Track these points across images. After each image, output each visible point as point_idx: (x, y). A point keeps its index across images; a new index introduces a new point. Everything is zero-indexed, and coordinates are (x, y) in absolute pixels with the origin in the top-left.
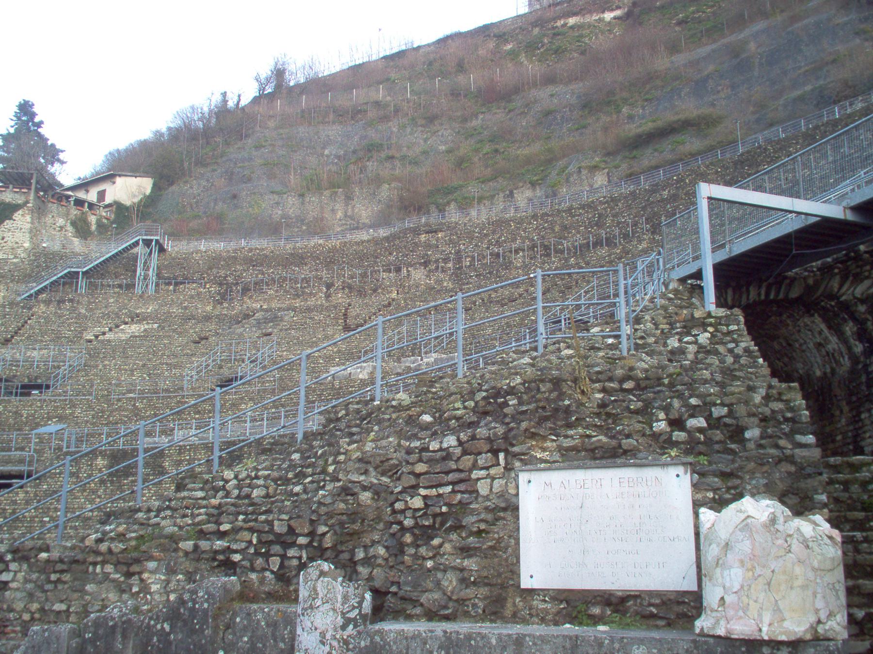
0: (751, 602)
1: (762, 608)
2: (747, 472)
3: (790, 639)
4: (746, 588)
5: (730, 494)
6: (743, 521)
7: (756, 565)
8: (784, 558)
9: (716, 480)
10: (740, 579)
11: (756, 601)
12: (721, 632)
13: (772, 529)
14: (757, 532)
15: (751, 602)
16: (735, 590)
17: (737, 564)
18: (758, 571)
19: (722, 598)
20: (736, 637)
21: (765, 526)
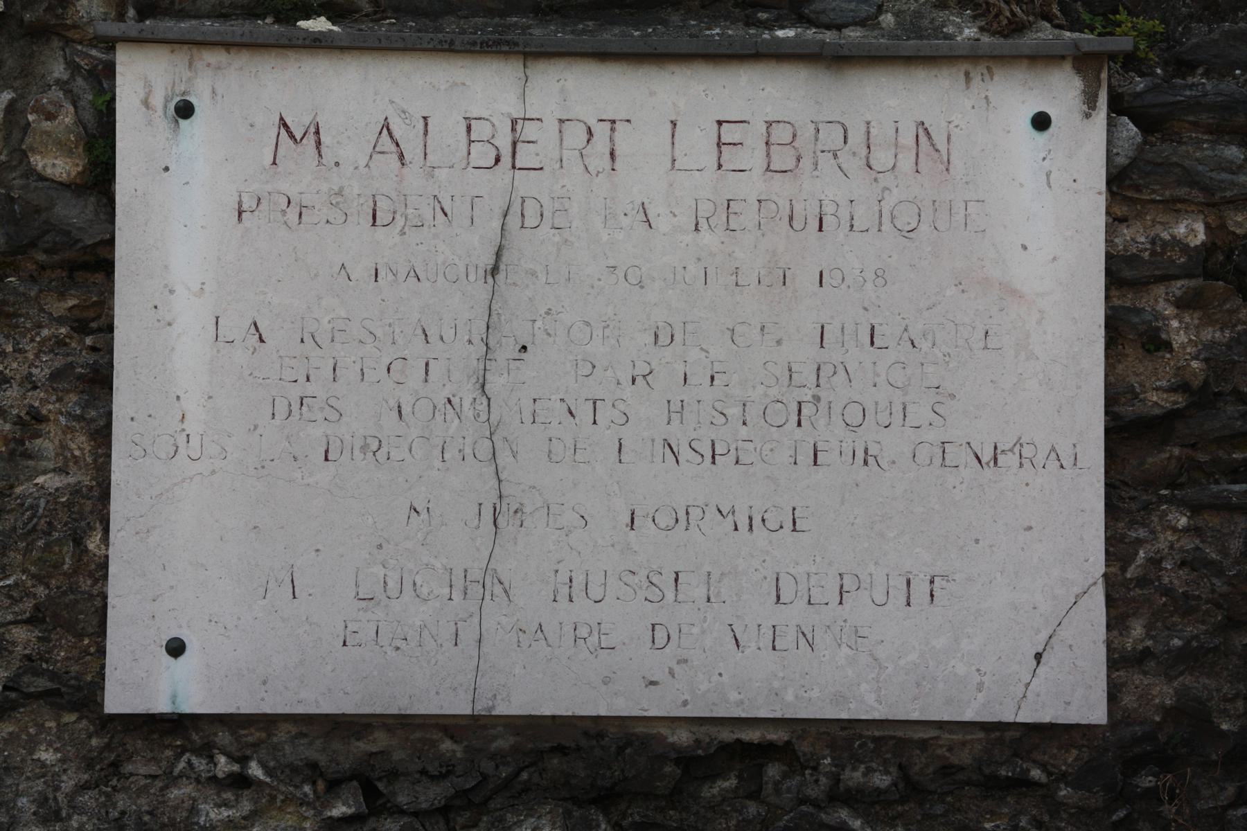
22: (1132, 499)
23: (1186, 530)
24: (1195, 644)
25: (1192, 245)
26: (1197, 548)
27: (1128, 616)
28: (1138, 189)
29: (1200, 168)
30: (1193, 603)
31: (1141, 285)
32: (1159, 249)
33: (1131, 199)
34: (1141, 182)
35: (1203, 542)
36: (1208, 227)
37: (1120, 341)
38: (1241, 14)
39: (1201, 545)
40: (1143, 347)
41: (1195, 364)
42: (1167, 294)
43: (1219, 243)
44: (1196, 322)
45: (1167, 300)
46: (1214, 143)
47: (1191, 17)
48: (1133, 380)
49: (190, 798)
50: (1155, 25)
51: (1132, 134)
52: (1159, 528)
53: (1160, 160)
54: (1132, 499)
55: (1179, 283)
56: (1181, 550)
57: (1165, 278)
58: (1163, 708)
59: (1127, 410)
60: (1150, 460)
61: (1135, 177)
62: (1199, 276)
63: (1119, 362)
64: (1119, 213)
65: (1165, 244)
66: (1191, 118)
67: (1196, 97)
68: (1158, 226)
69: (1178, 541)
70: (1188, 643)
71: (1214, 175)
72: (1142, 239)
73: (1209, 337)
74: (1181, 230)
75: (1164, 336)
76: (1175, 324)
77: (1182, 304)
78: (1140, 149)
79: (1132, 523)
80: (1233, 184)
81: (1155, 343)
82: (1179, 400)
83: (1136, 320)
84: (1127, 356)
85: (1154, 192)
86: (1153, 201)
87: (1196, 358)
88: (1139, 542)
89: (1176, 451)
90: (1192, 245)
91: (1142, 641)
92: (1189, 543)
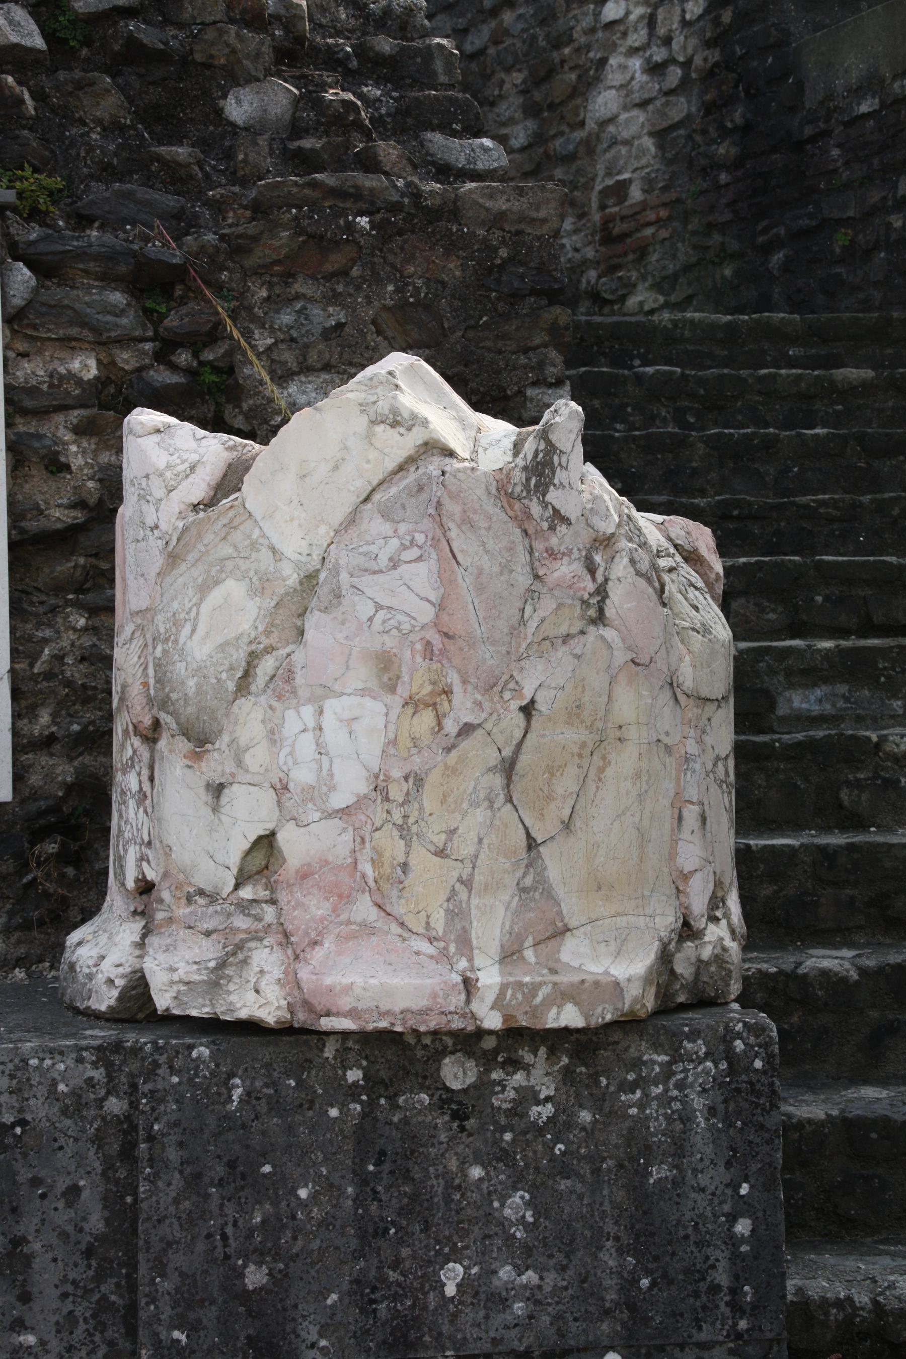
0: (421, 858)
1: (467, 883)
2: (257, 272)
3: (596, 1021)
4: (397, 792)
5: (174, 367)
6: (401, 468)
7: (453, 678)
8: (576, 645)
9: (117, 298)
10: (371, 750)
11: (440, 853)
12: (259, 997)
13: (536, 509)
14: (467, 522)
15: (421, 858)
16: (339, 801)
17: (361, 675)
18: (462, 708)
19: (266, 842)
20: (347, 1024)
21: (501, 489)
22: (42, 603)
23: (85, 629)
24: (91, 728)
25: (85, 379)
26: (94, 645)
27: (37, 706)
28: (35, 327)
29: (88, 310)
30: (90, 693)
31: (43, 413)
32: (56, 382)
33: (32, 337)
34: (38, 321)
35: (99, 639)
36: (99, 362)
37: (26, 463)
38: (135, 177)
39: (98, 643)
40: (46, 468)
41: (90, 484)
42: (66, 422)
43: (113, 378)
44: (93, 447)
45: (66, 427)
46: (103, 288)
47: (91, 176)
48: (40, 499)
49: (165, 1090)
50: (56, 182)
51: (26, 278)
52: (62, 628)
53: (53, 303)
54: (42, 603)
55: (76, 412)
56: (81, 647)
57: (63, 408)
58: (64, 783)
59: (32, 525)
60: (59, 568)
61: (31, 317)
62: (93, 406)
63: (27, 482)
64: (21, 349)
65: (61, 378)
66: (81, 266)
67: (82, 247)
68: (56, 362)
69: (78, 639)
70: (85, 728)
71: (100, 317)
72: (42, 373)
73: (106, 460)
74: (76, 365)
75: (63, 459)
76: (74, 448)
77: (79, 431)
78: (36, 291)
79: (39, 625)
80: (117, 325)
81: (56, 466)
82: (78, 516)
83: (37, 444)
84: (33, 476)
85: (49, 330)
86: (50, 339)
87: (91, 478)
88: (45, 641)
89: (82, 560)
90: (85, 379)
91: (48, 727)
92: (87, 641)
